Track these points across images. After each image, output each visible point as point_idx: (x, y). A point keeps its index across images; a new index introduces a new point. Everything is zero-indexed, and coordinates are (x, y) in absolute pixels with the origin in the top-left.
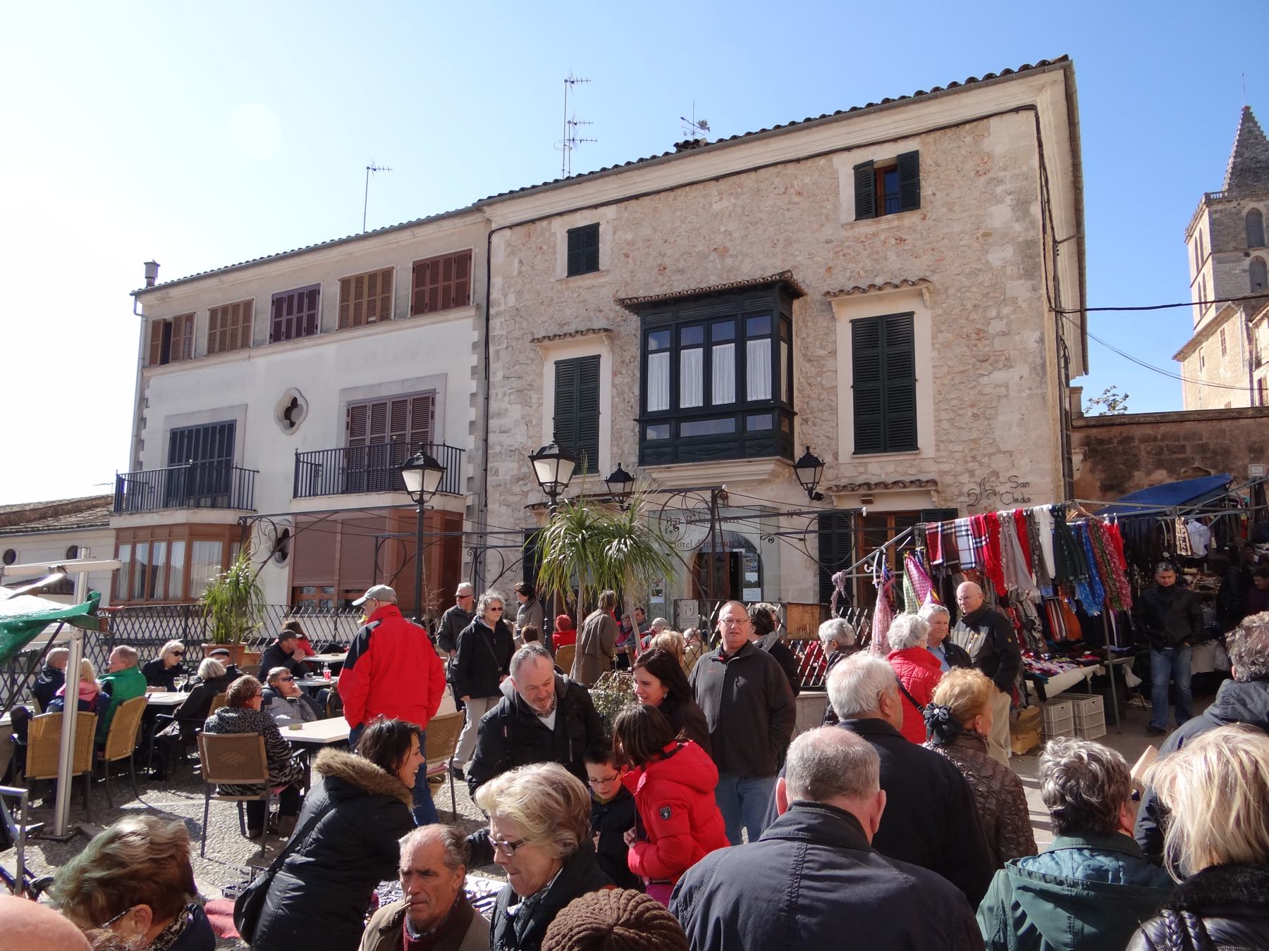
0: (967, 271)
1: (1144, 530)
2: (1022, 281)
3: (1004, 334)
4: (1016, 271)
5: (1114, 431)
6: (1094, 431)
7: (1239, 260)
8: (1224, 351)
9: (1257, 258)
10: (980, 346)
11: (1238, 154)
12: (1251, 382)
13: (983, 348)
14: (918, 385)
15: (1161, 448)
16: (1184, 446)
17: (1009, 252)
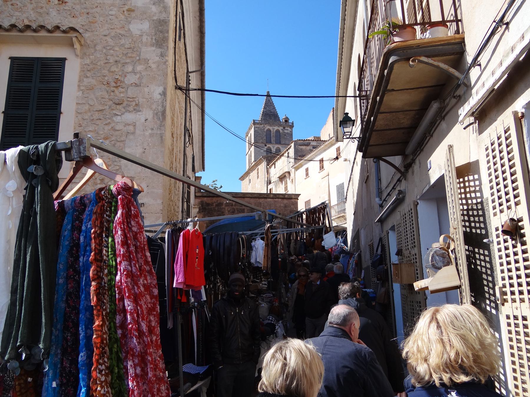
0: (113, 34)
1: (227, 243)
2: (154, 48)
3: (136, 85)
4: (150, 40)
5: (215, 199)
6: (205, 199)
8: (258, 177)
9: (269, 147)
10: (117, 92)
11: (265, 108)
12: (267, 190)
13: (119, 94)
14: (62, 117)
15: (234, 209)
16: (244, 209)
17: (146, 26)
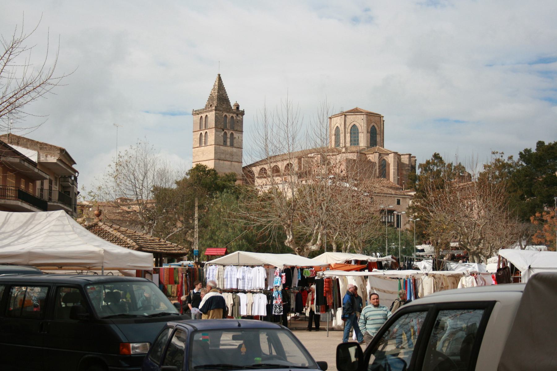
7: (221, 132)
